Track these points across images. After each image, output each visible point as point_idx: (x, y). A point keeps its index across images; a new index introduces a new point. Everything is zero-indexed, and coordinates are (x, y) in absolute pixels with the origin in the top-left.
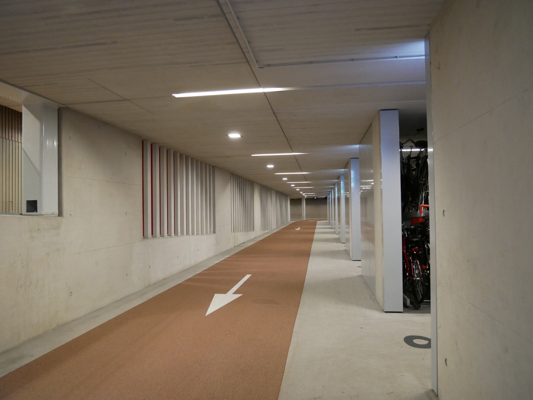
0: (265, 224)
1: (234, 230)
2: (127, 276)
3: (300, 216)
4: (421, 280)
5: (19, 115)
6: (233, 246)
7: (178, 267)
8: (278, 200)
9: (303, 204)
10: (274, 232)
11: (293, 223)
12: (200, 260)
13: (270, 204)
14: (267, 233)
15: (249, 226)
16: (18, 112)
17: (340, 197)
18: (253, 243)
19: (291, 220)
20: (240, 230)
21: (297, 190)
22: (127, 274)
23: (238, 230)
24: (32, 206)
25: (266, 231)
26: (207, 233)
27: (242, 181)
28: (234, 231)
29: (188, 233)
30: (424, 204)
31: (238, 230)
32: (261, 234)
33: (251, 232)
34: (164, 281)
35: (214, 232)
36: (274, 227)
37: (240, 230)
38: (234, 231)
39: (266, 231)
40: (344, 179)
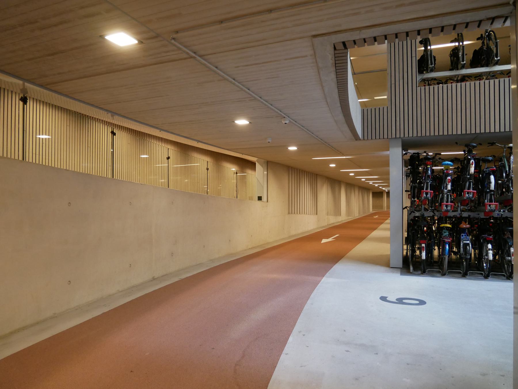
0: (349, 212)
1: (328, 214)
2: (204, 247)
3: (382, 207)
4: (457, 196)
5: (255, 164)
6: (327, 224)
7: (300, 231)
8: (360, 194)
9: (384, 196)
10: (331, 227)
11: (374, 213)
12: (310, 229)
13: (353, 195)
14: (351, 218)
15: (337, 212)
16: (254, 163)
17: (468, 277)
18: (322, 229)
19: (373, 211)
20: (331, 215)
21: (362, 180)
22: (130, 265)
23: (330, 215)
24: (260, 198)
25: (350, 217)
26: (313, 214)
27: (293, 176)
28: (327, 215)
29: (304, 214)
30: (430, 190)
31: (330, 215)
32: (345, 219)
33: (339, 217)
34: (295, 235)
35: (317, 214)
36: (356, 214)
37: (331, 215)
38: (327, 215)
39: (350, 217)
40: (400, 274)
